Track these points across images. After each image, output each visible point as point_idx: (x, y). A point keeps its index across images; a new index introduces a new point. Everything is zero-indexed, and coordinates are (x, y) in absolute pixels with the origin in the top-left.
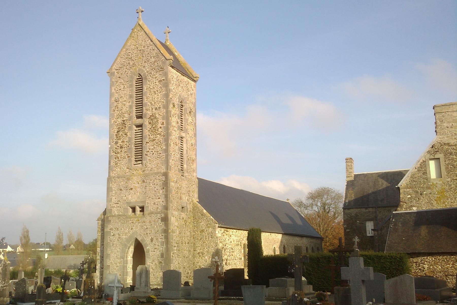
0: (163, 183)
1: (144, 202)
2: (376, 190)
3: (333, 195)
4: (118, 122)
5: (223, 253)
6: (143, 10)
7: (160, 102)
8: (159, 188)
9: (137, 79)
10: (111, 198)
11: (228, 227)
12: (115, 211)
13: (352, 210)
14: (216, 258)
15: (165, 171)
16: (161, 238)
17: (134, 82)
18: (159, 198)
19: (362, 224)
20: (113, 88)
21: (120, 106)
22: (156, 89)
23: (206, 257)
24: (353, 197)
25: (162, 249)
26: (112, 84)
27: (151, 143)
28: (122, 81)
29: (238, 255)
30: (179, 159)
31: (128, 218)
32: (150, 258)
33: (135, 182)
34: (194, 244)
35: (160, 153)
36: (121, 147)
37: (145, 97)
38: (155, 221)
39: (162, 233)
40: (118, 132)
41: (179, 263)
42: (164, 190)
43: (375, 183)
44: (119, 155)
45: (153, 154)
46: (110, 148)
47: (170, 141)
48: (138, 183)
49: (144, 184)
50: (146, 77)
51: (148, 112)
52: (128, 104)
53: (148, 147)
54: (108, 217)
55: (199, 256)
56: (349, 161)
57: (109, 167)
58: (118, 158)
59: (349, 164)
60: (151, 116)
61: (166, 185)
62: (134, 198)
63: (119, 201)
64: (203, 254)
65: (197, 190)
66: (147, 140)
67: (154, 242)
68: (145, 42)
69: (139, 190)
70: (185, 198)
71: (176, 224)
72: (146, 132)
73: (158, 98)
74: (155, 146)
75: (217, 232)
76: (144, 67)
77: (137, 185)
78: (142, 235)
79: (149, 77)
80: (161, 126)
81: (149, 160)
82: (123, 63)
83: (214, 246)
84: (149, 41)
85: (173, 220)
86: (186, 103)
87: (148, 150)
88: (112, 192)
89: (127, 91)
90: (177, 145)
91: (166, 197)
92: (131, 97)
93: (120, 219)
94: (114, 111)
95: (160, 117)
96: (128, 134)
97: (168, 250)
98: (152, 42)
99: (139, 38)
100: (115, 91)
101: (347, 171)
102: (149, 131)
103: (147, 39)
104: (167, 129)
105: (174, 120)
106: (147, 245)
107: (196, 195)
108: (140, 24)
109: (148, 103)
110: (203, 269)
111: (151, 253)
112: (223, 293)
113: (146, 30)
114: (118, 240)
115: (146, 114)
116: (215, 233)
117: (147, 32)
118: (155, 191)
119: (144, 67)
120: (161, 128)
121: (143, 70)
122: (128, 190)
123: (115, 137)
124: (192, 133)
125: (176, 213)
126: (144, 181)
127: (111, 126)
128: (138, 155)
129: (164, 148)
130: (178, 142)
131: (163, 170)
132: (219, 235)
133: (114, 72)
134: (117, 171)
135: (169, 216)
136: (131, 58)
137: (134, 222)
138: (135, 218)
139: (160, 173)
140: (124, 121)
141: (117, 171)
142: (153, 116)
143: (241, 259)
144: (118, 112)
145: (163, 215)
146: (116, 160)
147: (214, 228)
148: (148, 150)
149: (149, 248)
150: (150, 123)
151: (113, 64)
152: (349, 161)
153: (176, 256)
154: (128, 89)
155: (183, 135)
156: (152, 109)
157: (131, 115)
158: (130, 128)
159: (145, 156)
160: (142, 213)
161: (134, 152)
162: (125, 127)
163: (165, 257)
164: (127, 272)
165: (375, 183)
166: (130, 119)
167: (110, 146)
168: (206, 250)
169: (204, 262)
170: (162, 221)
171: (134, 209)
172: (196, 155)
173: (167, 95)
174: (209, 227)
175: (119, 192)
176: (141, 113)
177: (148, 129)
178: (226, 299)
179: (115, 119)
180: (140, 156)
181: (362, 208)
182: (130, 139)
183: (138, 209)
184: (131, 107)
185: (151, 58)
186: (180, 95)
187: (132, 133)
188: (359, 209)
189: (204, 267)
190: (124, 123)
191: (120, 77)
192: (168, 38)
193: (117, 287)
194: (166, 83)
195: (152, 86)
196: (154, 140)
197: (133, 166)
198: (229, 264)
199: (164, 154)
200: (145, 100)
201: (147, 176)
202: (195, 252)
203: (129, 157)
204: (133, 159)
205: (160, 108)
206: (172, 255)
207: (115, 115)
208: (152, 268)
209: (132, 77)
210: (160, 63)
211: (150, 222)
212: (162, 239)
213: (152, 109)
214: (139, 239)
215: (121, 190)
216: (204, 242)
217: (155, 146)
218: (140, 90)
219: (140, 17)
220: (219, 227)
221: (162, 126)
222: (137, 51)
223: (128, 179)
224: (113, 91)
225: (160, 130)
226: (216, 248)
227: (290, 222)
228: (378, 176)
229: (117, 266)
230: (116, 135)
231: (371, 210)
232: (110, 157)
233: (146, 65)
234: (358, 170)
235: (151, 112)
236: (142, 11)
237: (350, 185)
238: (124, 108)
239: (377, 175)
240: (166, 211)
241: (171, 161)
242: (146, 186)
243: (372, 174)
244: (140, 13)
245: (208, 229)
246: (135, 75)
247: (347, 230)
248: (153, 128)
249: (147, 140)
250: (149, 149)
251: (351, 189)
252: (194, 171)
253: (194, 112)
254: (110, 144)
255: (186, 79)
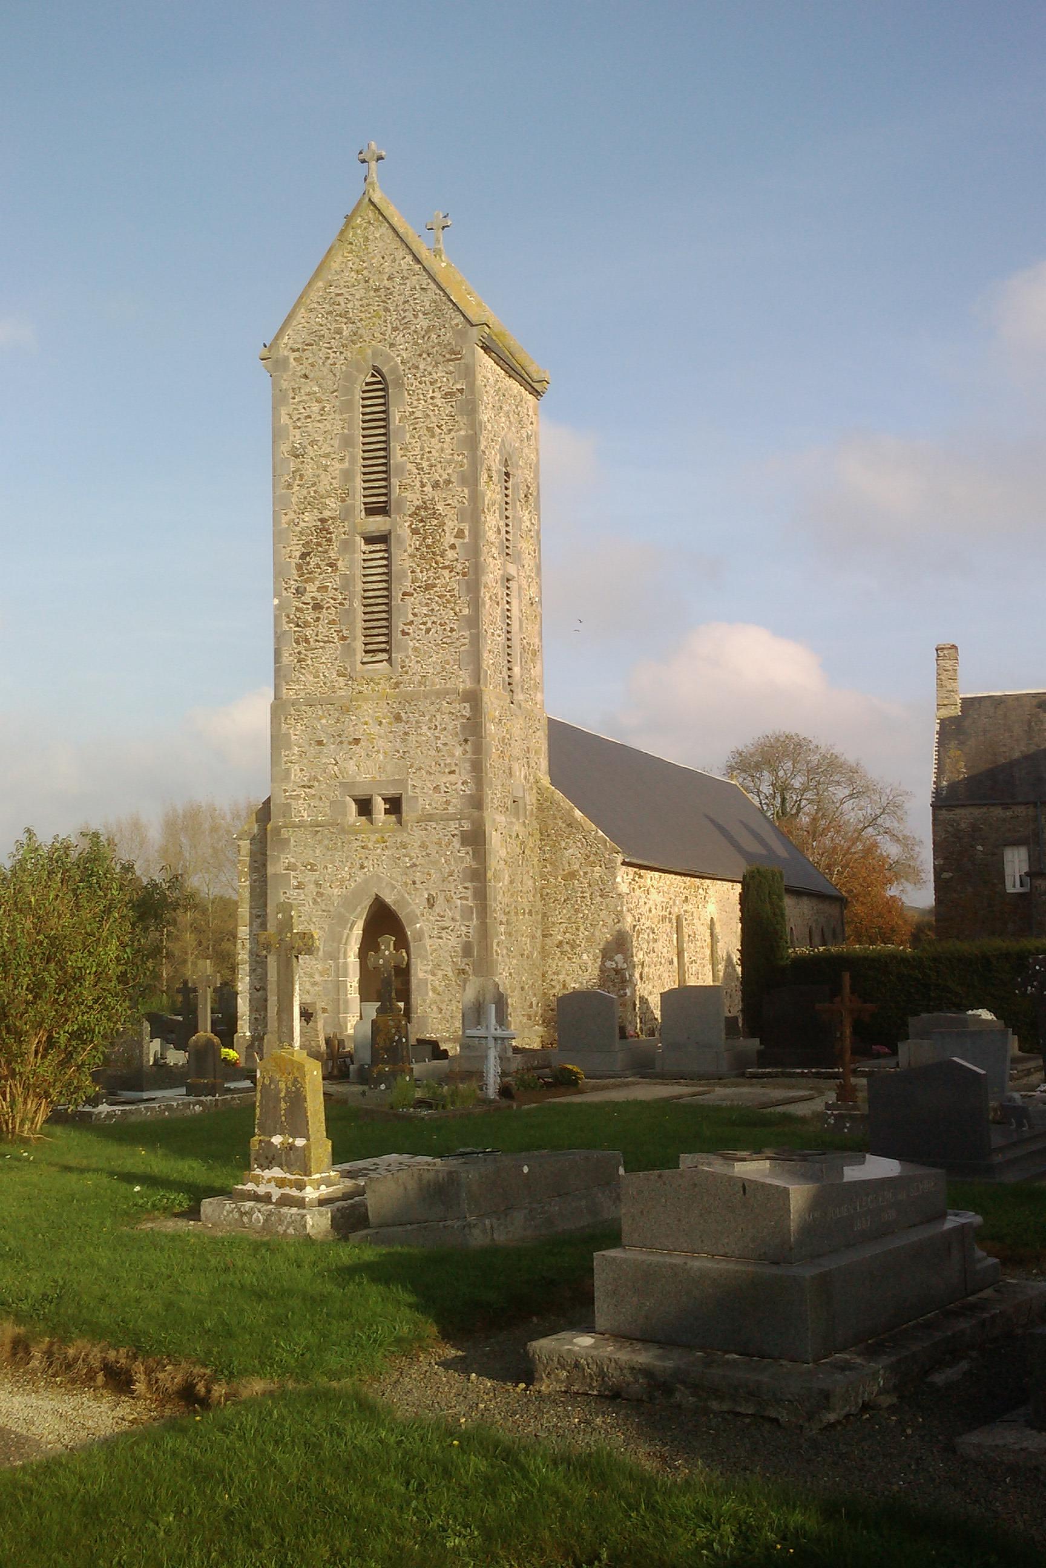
0: (463, 726)
1: (403, 782)
2: (1033, 749)
3: (815, 759)
4: (302, 524)
5: (635, 943)
6: (384, 153)
7: (449, 462)
8: (452, 741)
9: (367, 384)
10: (288, 770)
11: (646, 863)
12: (302, 812)
13: (958, 811)
14: (619, 957)
15: (469, 685)
16: (462, 895)
17: (358, 395)
18: (452, 772)
19: (994, 854)
20: (283, 411)
21: (309, 470)
22: (434, 419)
23: (585, 956)
24: (962, 772)
25: (468, 928)
26: (279, 399)
27: (418, 597)
28: (316, 389)
29: (665, 950)
30: (504, 650)
31: (348, 833)
32: (425, 958)
33: (368, 721)
34: (544, 915)
35: (452, 630)
36: (317, 607)
37: (395, 446)
38: (439, 844)
39: (464, 881)
40: (303, 556)
41: (510, 974)
42: (468, 747)
43: (1029, 726)
44: (308, 632)
45: (428, 631)
46: (278, 608)
47: (483, 590)
48: (380, 724)
49: (401, 727)
50: (399, 378)
51: (408, 495)
52: (337, 465)
53: (410, 607)
54: (277, 830)
55: (562, 953)
56: (946, 653)
57: (277, 671)
58: (307, 641)
59: (948, 664)
60: (418, 508)
61: (473, 729)
62: (367, 770)
63: (315, 779)
64: (573, 948)
65: (545, 747)
66: (407, 585)
67: (437, 909)
68: (394, 261)
69: (380, 743)
70: (520, 772)
71: (503, 853)
72: (403, 561)
73: (442, 450)
74: (434, 606)
75: (619, 879)
76: (392, 345)
77: (375, 729)
78: (398, 885)
79: (410, 380)
80: (453, 541)
81: (415, 649)
82: (318, 327)
83: (610, 922)
84: (409, 258)
85: (495, 840)
86: (518, 467)
87: (411, 617)
88: (290, 749)
89: (335, 424)
90: (498, 604)
91: (477, 768)
92: (347, 442)
93: (319, 837)
94: (289, 486)
95: (451, 513)
96: (340, 564)
97: (484, 932)
98: (418, 262)
99: (371, 248)
100: (289, 422)
101: (940, 685)
102: (412, 556)
103: (402, 252)
104: (474, 551)
105: (491, 521)
106: (414, 919)
107: (544, 764)
108: (376, 200)
109: (409, 466)
110: (576, 994)
111: (428, 942)
112: (763, 1059)
113: (395, 221)
114: (315, 902)
115: (401, 502)
116: (614, 882)
117: (401, 230)
118: (438, 750)
119: (392, 345)
120: (453, 547)
121: (388, 356)
122: (345, 745)
123: (295, 571)
124: (532, 563)
125: (501, 819)
126: (398, 718)
127: (279, 536)
128: (376, 632)
129: (466, 611)
130: (501, 592)
131: (463, 682)
132: (624, 888)
133: (287, 358)
134: (305, 683)
135: (488, 828)
136: (344, 314)
137: (370, 845)
138: (374, 832)
139: (456, 691)
140: (321, 520)
141: (305, 683)
142: (426, 508)
143: (671, 962)
144: (305, 492)
145: (467, 826)
146: (301, 648)
147: (610, 868)
148: (411, 617)
149: (420, 924)
150: (415, 532)
151: (282, 330)
152: (946, 653)
153: (505, 952)
154: (338, 417)
155: (512, 570)
156: (423, 486)
157: (349, 501)
158: (347, 546)
159: (400, 636)
160: (393, 818)
161: (360, 625)
162: (330, 540)
163: (476, 954)
164: (346, 1001)
165: (1029, 726)
166: (347, 513)
167: (276, 601)
168: (583, 933)
169: (580, 972)
170: (463, 844)
171: (365, 807)
172: (540, 633)
173: (472, 442)
174: (592, 864)
175: (313, 749)
176: (383, 499)
177: (410, 550)
178: (776, 1076)
179: (292, 515)
180: (382, 637)
181: (993, 805)
182: (347, 582)
183: (379, 805)
184: (347, 475)
185: (416, 316)
186: (503, 441)
187: (352, 561)
188: (984, 810)
189: (577, 986)
190: (323, 528)
191: (306, 376)
192: (441, 246)
193: (496, 1039)
194: (468, 401)
195: (416, 408)
196: (428, 587)
197: (359, 666)
198: (649, 979)
199: (467, 634)
200: (397, 457)
201: (408, 700)
202: (548, 940)
203: (344, 638)
204: (359, 645)
205: (448, 482)
206: (495, 947)
207: (294, 500)
208: (434, 990)
209: (349, 377)
210: (448, 336)
211: (423, 846)
212: (466, 899)
213: (423, 486)
214: (389, 899)
215: (320, 743)
216: (577, 911)
217: (434, 606)
218: (379, 422)
219: (374, 177)
220: (624, 863)
221: (458, 542)
222: (367, 290)
223: (345, 710)
224: (284, 419)
225: (451, 554)
226: (617, 927)
227: (764, 852)
228: (1039, 706)
229: (314, 984)
230: (299, 567)
231: (1020, 810)
232: (279, 637)
233: (400, 339)
234: (977, 681)
235: (418, 496)
236: (380, 158)
237: (950, 731)
238: (325, 479)
239: (1035, 702)
240: (476, 813)
241: (485, 655)
242: (406, 734)
243: (1018, 698)
244: (373, 164)
245: (589, 869)
246: (359, 371)
247: (946, 875)
248: (428, 546)
249: (407, 585)
250: (415, 615)
251: (953, 744)
252: (536, 686)
253: (535, 494)
254: (277, 594)
255: (516, 387)
